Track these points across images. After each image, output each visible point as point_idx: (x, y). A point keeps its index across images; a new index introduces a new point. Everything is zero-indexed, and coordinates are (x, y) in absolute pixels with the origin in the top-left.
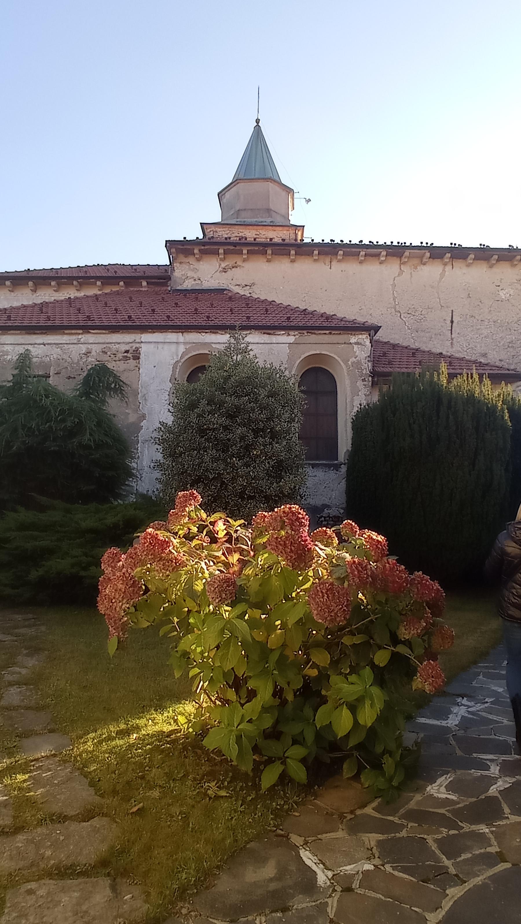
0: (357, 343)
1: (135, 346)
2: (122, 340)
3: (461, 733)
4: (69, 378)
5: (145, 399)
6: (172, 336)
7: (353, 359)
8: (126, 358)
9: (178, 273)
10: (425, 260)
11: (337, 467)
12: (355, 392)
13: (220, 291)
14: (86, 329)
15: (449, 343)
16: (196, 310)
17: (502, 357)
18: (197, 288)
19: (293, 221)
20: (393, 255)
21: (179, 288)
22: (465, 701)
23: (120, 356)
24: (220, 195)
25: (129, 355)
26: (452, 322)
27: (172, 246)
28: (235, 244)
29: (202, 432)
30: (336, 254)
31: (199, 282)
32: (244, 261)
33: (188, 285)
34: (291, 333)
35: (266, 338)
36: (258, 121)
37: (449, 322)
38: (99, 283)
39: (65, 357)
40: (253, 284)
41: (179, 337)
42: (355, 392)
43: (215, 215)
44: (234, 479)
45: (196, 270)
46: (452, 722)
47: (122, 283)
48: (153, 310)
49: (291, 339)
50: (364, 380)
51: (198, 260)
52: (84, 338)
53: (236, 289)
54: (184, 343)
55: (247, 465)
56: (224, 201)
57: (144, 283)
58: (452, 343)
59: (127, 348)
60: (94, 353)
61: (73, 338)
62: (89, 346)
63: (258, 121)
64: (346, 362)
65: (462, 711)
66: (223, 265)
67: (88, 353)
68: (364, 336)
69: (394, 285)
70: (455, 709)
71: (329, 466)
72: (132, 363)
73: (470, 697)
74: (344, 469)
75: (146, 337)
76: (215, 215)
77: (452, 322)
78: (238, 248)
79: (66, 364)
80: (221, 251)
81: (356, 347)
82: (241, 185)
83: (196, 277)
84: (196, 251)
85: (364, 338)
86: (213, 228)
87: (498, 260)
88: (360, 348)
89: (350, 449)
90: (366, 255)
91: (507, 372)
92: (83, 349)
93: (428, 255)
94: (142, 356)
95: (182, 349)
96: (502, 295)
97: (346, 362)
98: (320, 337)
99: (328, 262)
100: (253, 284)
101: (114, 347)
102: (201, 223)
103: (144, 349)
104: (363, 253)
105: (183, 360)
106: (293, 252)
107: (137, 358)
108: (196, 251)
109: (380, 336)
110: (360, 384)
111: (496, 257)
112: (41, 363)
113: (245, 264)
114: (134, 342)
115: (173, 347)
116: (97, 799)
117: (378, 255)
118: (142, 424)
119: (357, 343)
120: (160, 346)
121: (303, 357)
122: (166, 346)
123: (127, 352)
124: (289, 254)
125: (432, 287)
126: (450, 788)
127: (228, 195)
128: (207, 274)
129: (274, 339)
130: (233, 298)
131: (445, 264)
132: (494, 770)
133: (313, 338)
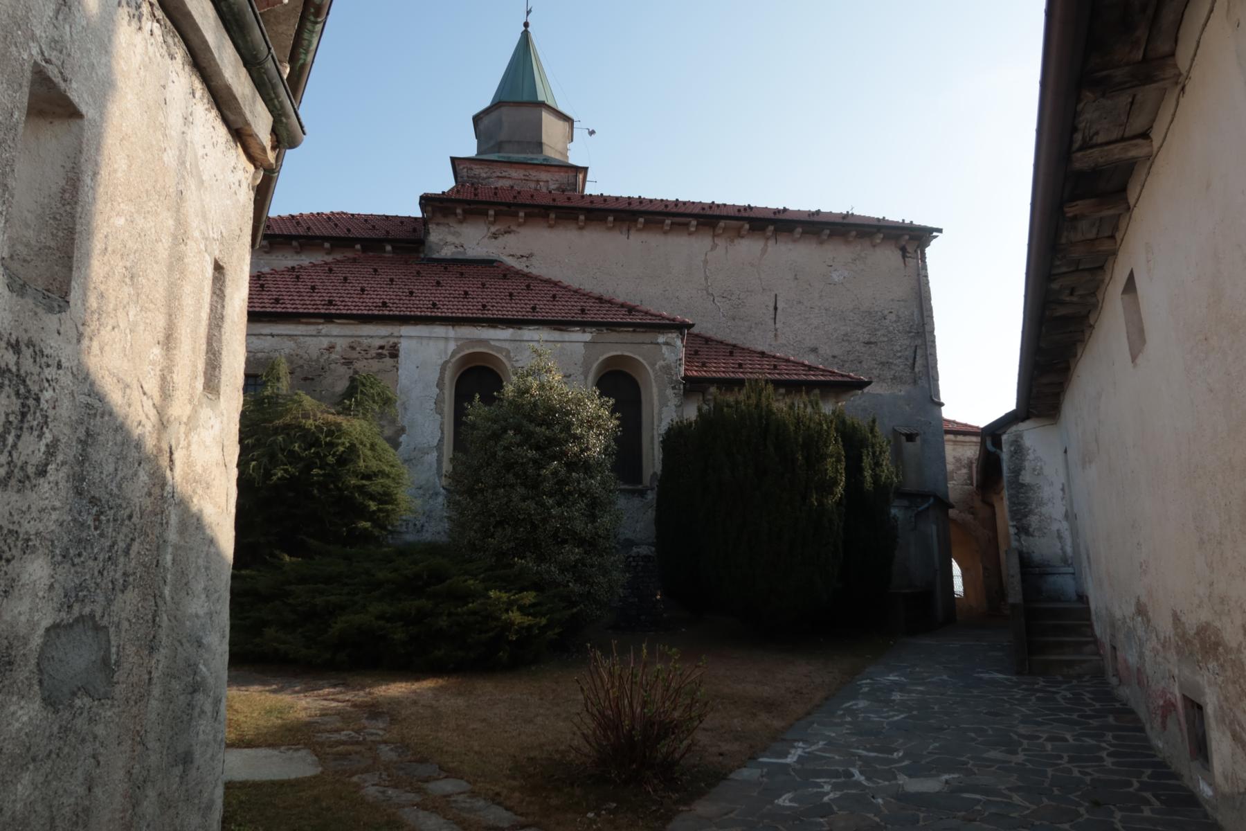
0: (667, 344)
1: (392, 340)
2: (376, 334)
3: (798, 767)
4: (306, 379)
5: (405, 409)
6: (440, 330)
7: (661, 363)
8: (380, 356)
9: (436, 235)
10: (743, 232)
11: (642, 494)
12: (664, 402)
13: (488, 263)
14: (329, 318)
15: (771, 334)
16: (466, 293)
17: (836, 353)
18: (460, 257)
19: (575, 159)
20: (704, 224)
21: (435, 256)
22: (801, 744)
23: (373, 352)
24: (477, 119)
25: (385, 352)
26: (776, 309)
27: (427, 201)
28: (509, 205)
29: (509, 467)
30: (636, 221)
31: (461, 249)
32: (520, 225)
33: (447, 252)
34: (588, 329)
35: (556, 335)
36: (526, 25)
37: (772, 308)
38: (327, 245)
39: (301, 352)
40: (531, 255)
41: (450, 332)
42: (664, 402)
43: (468, 147)
44: (545, 521)
45: (455, 234)
46: (790, 759)
47: (358, 247)
48: (411, 293)
49: (587, 337)
50: (674, 388)
51: (461, 222)
52: (325, 328)
53: (511, 262)
54: (456, 339)
55: (559, 504)
56: (482, 127)
57: (389, 248)
58: (776, 335)
59: (382, 342)
60: (338, 348)
61: (311, 329)
62: (333, 340)
63: (526, 25)
64: (653, 365)
65: (799, 752)
66: (493, 229)
67: (331, 348)
68: (674, 335)
69: (706, 262)
70: (793, 751)
71: (633, 492)
72: (389, 361)
73: (805, 741)
74: (651, 496)
75: (406, 330)
76: (468, 147)
77: (776, 309)
78: (513, 209)
79: (301, 362)
80: (491, 212)
81: (664, 348)
82: (504, 110)
83: (457, 242)
84: (459, 211)
85: (674, 337)
86: (468, 164)
87: (830, 236)
88: (672, 352)
89: (659, 473)
90: (672, 224)
91: (840, 379)
92: (325, 342)
93: (747, 226)
94: (402, 354)
95: (452, 346)
96: (835, 276)
97: (653, 365)
98: (622, 335)
99: (625, 229)
100: (531, 255)
101: (365, 341)
102: (453, 160)
103: (404, 345)
104: (668, 222)
105: (454, 360)
106: (582, 217)
107: (394, 354)
108: (459, 211)
109: (695, 330)
110: (669, 392)
111: (828, 232)
112: (267, 359)
113: (519, 230)
114: (391, 335)
115: (441, 344)
116: (515, 817)
117: (687, 225)
118: (401, 439)
119: (667, 344)
120: (425, 342)
121: (601, 358)
122: (432, 343)
123: (382, 347)
124: (577, 219)
125: (752, 265)
126: (791, 801)
127: (486, 121)
128: (471, 240)
129: (567, 336)
130: (507, 273)
131: (768, 239)
132: (827, 788)
133: (613, 336)
